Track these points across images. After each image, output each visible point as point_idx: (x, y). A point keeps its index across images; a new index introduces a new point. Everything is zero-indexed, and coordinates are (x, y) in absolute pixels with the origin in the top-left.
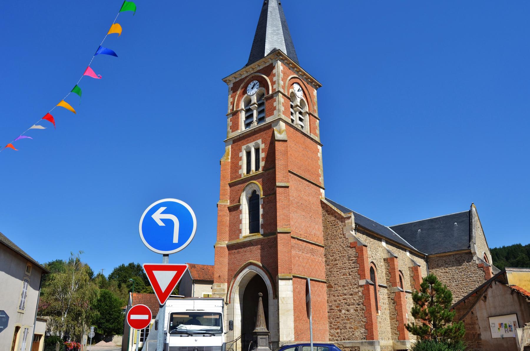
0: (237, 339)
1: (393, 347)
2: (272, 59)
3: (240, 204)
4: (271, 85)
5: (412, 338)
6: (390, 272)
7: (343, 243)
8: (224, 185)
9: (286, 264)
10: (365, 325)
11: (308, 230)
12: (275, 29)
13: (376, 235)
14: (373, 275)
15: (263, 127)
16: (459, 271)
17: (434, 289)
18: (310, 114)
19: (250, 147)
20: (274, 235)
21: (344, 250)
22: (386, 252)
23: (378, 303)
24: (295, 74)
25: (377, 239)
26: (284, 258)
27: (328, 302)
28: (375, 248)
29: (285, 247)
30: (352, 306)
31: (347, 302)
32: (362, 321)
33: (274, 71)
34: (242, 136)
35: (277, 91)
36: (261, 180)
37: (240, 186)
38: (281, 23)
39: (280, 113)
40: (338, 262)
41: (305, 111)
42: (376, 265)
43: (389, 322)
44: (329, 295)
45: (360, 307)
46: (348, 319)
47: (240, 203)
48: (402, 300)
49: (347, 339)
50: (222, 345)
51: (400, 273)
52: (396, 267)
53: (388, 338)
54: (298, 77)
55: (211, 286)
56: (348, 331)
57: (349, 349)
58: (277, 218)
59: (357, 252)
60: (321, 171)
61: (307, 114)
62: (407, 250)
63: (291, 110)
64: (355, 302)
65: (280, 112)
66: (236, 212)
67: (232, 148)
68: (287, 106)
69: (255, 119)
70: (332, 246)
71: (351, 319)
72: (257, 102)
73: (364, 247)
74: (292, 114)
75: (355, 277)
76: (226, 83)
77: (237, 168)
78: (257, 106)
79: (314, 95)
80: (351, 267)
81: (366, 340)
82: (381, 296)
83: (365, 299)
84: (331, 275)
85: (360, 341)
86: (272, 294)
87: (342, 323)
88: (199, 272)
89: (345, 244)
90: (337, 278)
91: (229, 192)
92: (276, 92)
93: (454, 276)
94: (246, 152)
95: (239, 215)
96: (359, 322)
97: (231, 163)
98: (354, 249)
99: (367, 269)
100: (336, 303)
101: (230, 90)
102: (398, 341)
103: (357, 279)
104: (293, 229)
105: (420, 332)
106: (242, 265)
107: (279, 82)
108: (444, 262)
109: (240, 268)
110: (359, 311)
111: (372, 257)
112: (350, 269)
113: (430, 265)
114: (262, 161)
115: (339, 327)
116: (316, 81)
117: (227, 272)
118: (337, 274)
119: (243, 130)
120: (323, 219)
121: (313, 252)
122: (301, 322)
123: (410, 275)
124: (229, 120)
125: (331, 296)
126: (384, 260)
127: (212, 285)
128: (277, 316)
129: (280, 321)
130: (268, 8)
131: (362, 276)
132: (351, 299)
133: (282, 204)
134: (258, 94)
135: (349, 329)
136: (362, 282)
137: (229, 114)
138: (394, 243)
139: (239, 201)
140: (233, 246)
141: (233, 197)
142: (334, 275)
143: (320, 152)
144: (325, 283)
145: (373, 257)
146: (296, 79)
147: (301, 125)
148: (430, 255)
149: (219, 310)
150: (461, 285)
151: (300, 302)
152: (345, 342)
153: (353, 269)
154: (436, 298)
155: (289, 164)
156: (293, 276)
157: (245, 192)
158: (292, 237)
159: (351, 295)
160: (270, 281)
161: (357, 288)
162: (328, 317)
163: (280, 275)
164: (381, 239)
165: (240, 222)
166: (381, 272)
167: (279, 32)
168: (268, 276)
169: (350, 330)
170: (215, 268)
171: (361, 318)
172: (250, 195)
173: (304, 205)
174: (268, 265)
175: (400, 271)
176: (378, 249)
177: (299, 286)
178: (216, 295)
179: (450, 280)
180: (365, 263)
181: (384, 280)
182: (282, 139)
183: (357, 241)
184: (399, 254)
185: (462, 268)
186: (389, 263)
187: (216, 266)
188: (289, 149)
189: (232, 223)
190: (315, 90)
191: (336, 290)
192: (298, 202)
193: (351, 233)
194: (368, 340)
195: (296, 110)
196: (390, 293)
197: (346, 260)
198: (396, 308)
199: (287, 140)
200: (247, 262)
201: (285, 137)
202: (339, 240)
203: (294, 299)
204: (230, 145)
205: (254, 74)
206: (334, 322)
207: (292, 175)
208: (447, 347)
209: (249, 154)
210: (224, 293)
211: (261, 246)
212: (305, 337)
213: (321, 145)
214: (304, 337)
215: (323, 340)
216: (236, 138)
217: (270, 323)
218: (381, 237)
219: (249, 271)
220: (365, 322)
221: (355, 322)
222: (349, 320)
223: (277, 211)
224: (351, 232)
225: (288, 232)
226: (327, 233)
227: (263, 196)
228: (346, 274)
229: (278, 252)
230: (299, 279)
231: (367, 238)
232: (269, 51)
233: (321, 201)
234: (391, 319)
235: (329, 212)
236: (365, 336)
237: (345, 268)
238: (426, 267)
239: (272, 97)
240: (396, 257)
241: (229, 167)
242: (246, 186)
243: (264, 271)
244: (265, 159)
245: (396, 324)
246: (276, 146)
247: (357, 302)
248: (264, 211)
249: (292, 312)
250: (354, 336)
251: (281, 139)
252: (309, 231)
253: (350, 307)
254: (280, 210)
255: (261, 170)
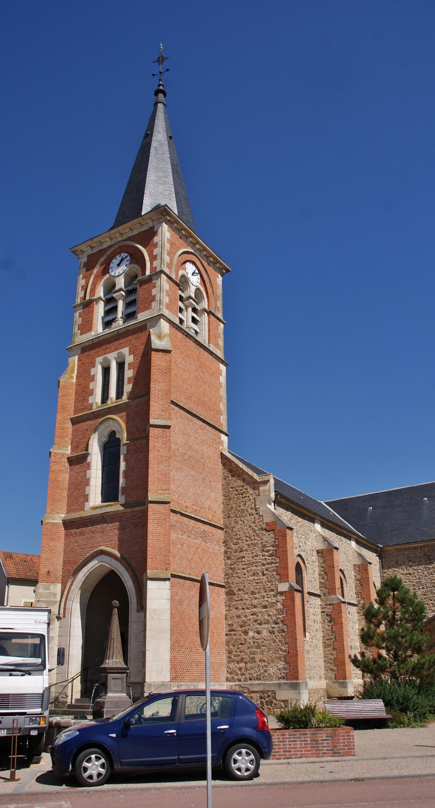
0: (74, 678)
1: (327, 691)
2: (153, 220)
3: (88, 453)
4: (150, 260)
5: (356, 676)
6: (327, 572)
7: (254, 523)
8: (63, 421)
9: (160, 555)
10: (285, 657)
11: (199, 501)
12: (161, 174)
13: (306, 512)
14: (300, 576)
15: (132, 328)
16: (428, 572)
17: (398, 599)
18: (210, 313)
19: (110, 360)
20: (143, 505)
21: (255, 534)
22: (321, 540)
23: (306, 621)
24: (188, 247)
25: (307, 518)
26: (157, 544)
27: (226, 619)
28: (304, 532)
29: (161, 526)
30: (266, 626)
31: (257, 618)
32: (281, 650)
33: (156, 239)
34: (97, 341)
35: (159, 271)
36: (124, 414)
37: (89, 423)
38: (170, 167)
39: (161, 306)
40: (246, 554)
41: (202, 308)
42: (305, 559)
43: (322, 652)
44: (229, 606)
45: (279, 627)
46: (258, 647)
47: (87, 451)
48: (343, 616)
49: (255, 679)
50: (44, 691)
51: (340, 573)
52: (335, 563)
53: (319, 677)
54: (193, 252)
55: (33, 588)
56: (257, 665)
57: (258, 695)
58: (149, 477)
59: (276, 537)
60: (224, 405)
61: (205, 313)
62: (353, 538)
63: (180, 304)
64: (270, 618)
65: (161, 304)
66: (80, 467)
67: (79, 360)
68: (173, 297)
69: (120, 314)
70: (236, 528)
71: (263, 646)
72: (125, 287)
73: (288, 531)
74: (181, 310)
75: (272, 579)
76: (76, 255)
77: (86, 393)
78: (124, 294)
79: (217, 284)
80: (265, 562)
81: (287, 680)
82: (311, 610)
83: (286, 615)
84: (233, 574)
85: (277, 682)
86: (136, 604)
87: (248, 652)
88: (17, 566)
89: (257, 525)
90: (242, 579)
91: (70, 433)
92: (157, 272)
93: (420, 580)
94: (102, 367)
95: (85, 471)
96: (276, 651)
97: (76, 385)
98: (272, 533)
99: (292, 566)
100: (240, 620)
101: (82, 266)
102: (335, 681)
103: (275, 582)
104: (175, 497)
105: (374, 669)
106: (88, 555)
107: (163, 256)
108: (407, 558)
109: (83, 559)
110: (276, 633)
111: (300, 547)
112: (264, 565)
113: (384, 562)
114: (129, 383)
115: (243, 659)
116: (222, 262)
117: (60, 565)
118: (243, 573)
119: (99, 332)
120: (224, 484)
121: (205, 537)
122: (182, 651)
123: (355, 576)
124: (77, 314)
125: (231, 609)
126: (318, 552)
127: (35, 587)
128: (143, 640)
129: (147, 649)
130: (151, 142)
131: (284, 578)
132: (264, 614)
133: (157, 455)
134: (127, 275)
135: (259, 663)
136: (283, 587)
137: (78, 305)
138: (333, 526)
139: (87, 448)
140: (73, 522)
141: (76, 441)
142: (238, 575)
143: (222, 375)
144: (223, 588)
145: (301, 547)
146: (190, 255)
147: (194, 330)
148: (386, 547)
149: (42, 629)
150: (431, 593)
151: (181, 617)
152: (252, 683)
153: (269, 566)
154: (401, 613)
155: (172, 391)
156: (171, 574)
157: (97, 433)
158: (173, 511)
159: (265, 607)
160: (134, 583)
161: (274, 597)
162: (226, 642)
163: (150, 573)
164: (314, 519)
165: (87, 482)
166: (312, 571)
167: (167, 180)
168: (129, 574)
169: (260, 664)
170: (42, 558)
171: (279, 645)
172: (104, 439)
173: (194, 458)
174: (130, 556)
175: (341, 570)
176: (308, 534)
177: (180, 592)
178: (42, 603)
179: (414, 585)
180: (288, 555)
181: (317, 584)
182: (163, 349)
183: (277, 520)
184: (339, 544)
185: (433, 568)
186: (325, 558)
187: (43, 555)
188: (173, 365)
189: (74, 484)
190: (220, 276)
191: (240, 598)
192: (185, 454)
193: (268, 507)
194: (289, 680)
195: (187, 305)
196: (326, 605)
197: (258, 551)
198: (334, 630)
199: (171, 351)
200: (96, 550)
201: (168, 346)
202: (249, 518)
203: (172, 612)
204: (76, 355)
205: (122, 242)
206: (236, 651)
207: (177, 409)
208: (417, 692)
209: (106, 371)
210: (55, 600)
211: (119, 524)
212: (187, 676)
213: (226, 365)
214: (185, 676)
215: (216, 680)
216: (87, 344)
217: (130, 652)
218: (315, 516)
219: (99, 564)
220: (285, 651)
221: (268, 651)
222: (260, 648)
223: (149, 465)
224: (268, 505)
225: (166, 501)
226: (230, 506)
227: (127, 441)
228: (258, 573)
229: (147, 534)
230: (181, 581)
231: (292, 516)
232: (149, 207)
233: (222, 453)
234: (326, 646)
235: (234, 473)
236: (284, 675)
237: (257, 564)
238: (379, 565)
239: (150, 279)
240: (337, 549)
241: (72, 391)
242: (100, 424)
243: (123, 564)
244: (132, 381)
245: (332, 655)
246: (152, 358)
247: (274, 618)
248: (127, 466)
249: (167, 635)
250: (267, 674)
251: (161, 348)
252: (201, 501)
253: (262, 626)
254: (155, 464)
255: (125, 398)
